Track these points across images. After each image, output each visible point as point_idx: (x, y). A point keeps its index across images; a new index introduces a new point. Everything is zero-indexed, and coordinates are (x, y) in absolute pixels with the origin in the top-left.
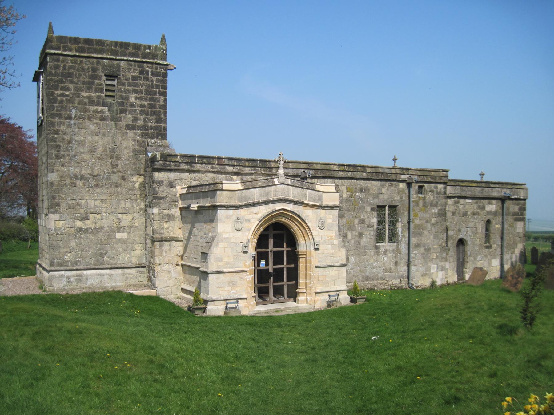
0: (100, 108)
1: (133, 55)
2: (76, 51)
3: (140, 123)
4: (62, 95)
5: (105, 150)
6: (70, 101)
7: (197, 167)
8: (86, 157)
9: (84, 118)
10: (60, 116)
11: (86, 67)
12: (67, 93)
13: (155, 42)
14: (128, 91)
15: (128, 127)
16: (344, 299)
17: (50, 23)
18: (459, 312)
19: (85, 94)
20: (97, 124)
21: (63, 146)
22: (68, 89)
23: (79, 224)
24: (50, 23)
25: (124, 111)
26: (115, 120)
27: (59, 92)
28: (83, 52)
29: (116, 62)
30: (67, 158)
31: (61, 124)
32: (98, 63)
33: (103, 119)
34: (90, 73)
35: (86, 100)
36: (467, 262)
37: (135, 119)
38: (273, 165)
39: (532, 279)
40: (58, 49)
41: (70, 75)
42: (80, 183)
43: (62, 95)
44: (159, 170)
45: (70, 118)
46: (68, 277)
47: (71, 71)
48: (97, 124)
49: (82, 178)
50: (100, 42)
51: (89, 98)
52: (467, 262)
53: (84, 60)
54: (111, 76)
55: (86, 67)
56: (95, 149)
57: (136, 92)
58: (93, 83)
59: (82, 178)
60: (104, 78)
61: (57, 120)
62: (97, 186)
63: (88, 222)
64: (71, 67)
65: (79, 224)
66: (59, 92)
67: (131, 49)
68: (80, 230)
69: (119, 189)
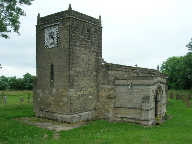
0: (85, 43)
1: (94, 22)
2: (79, 18)
3: (96, 50)
5: (86, 61)
6: (77, 39)
7: (118, 69)
8: (81, 64)
9: (81, 47)
10: (74, 45)
13: (97, 18)
14: (92, 37)
15: (93, 52)
17: (70, 4)
18: (103, 108)
19: (81, 37)
20: (84, 50)
21: (75, 58)
22: (76, 34)
23: (79, 93)
24: (70, 4)
25: (91, 45)
26: (90, 48)
27: (74, 35)
28: (80, 18)
29: (90, 25)
30: (76, 64)
31: (74, 49)
32: (85, 24)
33: (86, 48)
34: (83, 28)
35: (82, 39)
37: (95, 49)
40: (73, 16)
41: (77, 28)
42: (79, 75)
43: (75, 36)
44: (110, 70)
45: (77, 46)
46: (77, 117)
47: (77, 26)
48: (84, 50)
49: (80, 73)
51: (82, 38)
54: (89, 30)
55: (82, 25)
57: (95, 37)
58: (83, 32)
59: (80, 73)
60: (87, 31)
61: (73, 47)
62: (84, 76)
63: (82, 92)
64: (77, 25)
65: (79, 93)
66: (74, 35)
67: (93, 20)
68: (80, 96)
69: (90, 78)
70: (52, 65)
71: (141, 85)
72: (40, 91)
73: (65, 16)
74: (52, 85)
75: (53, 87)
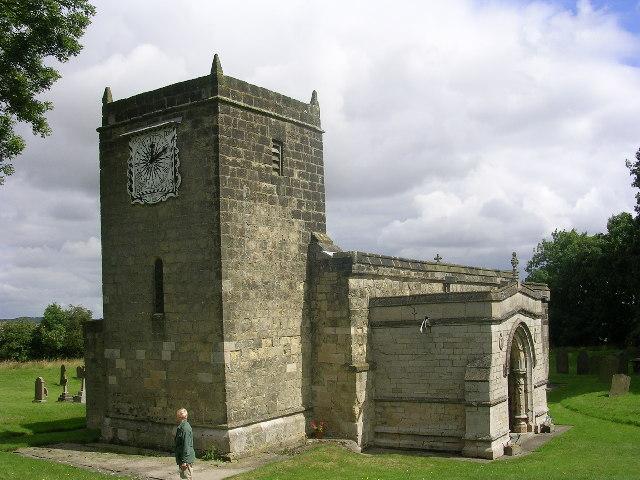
4: (234, 163)
11: (255, 126)
12: (239, 160)
16: (605, 232)
17: (216, 56)
19: (255, 164)
23: (253, 355)
24: (216, 56)
26: (284, 203)
29: (281, 122)
31: (234, 205)
36: (544, 240)
38: (429, 268)
39: (8, 141)
42: (252, 294)
45: (241, 198)
46: (248, 436)
50: (265, 92)
51: (259, 169)
52: (554, 235)
53: (253, 115)
54: (278, 143)
56: (17, 148)
57: (300, 166)
58: (262, 149)
59: (254, 286)
63: (261, 351)
64: (241, 123)
65: (253, 355)
68: (255, 364)
70: (159, 264)
71: (458, 321)
72: (117, 352)
73: (200, 95)
74: (159, 325)
75: (164, 338)
